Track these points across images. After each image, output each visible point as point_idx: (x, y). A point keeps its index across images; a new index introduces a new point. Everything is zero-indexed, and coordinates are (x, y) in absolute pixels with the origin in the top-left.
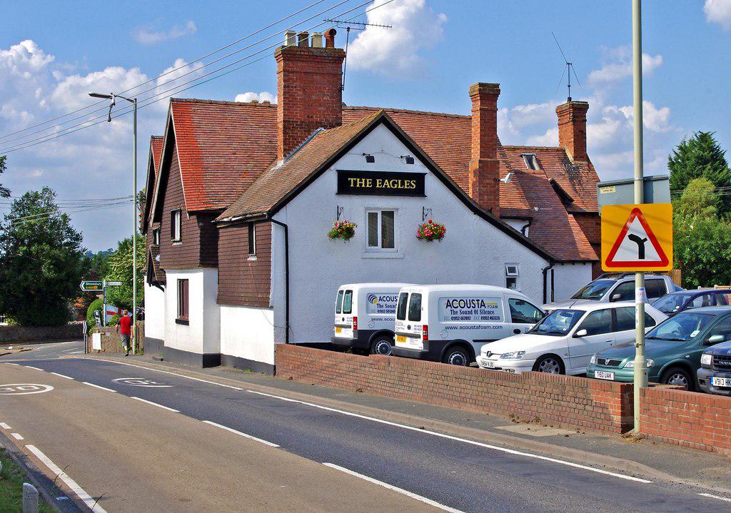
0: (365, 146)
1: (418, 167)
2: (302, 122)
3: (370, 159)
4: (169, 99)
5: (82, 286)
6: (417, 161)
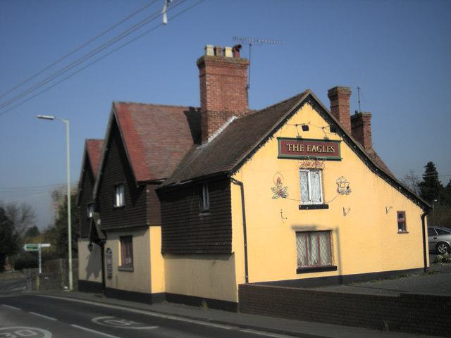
2: (220, 112)
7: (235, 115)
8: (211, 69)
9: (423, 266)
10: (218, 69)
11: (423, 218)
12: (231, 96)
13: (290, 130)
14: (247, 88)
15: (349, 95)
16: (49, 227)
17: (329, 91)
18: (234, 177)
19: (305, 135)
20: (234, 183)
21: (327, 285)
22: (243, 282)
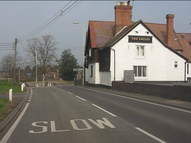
0: (136, 29)
1: (150, 35)
2: (121, 25)
3: (137, 32)
4: (178, 68)
5: (74, 70)
6: (149, 33)
7: (126, 26)
8: (118, 10)
9: (184, 80)
10: (121, 10)
11: (185, 63)
12: (125, 19)
13: (132, 33)
14: (131, 16)
15: (173, 17)
16: (76, 60)
17: (166, 16)
18: (112, 48)
19: (137, 35)
20: (112, 50)
21: (163, 83)
22: (113, 80)
